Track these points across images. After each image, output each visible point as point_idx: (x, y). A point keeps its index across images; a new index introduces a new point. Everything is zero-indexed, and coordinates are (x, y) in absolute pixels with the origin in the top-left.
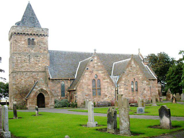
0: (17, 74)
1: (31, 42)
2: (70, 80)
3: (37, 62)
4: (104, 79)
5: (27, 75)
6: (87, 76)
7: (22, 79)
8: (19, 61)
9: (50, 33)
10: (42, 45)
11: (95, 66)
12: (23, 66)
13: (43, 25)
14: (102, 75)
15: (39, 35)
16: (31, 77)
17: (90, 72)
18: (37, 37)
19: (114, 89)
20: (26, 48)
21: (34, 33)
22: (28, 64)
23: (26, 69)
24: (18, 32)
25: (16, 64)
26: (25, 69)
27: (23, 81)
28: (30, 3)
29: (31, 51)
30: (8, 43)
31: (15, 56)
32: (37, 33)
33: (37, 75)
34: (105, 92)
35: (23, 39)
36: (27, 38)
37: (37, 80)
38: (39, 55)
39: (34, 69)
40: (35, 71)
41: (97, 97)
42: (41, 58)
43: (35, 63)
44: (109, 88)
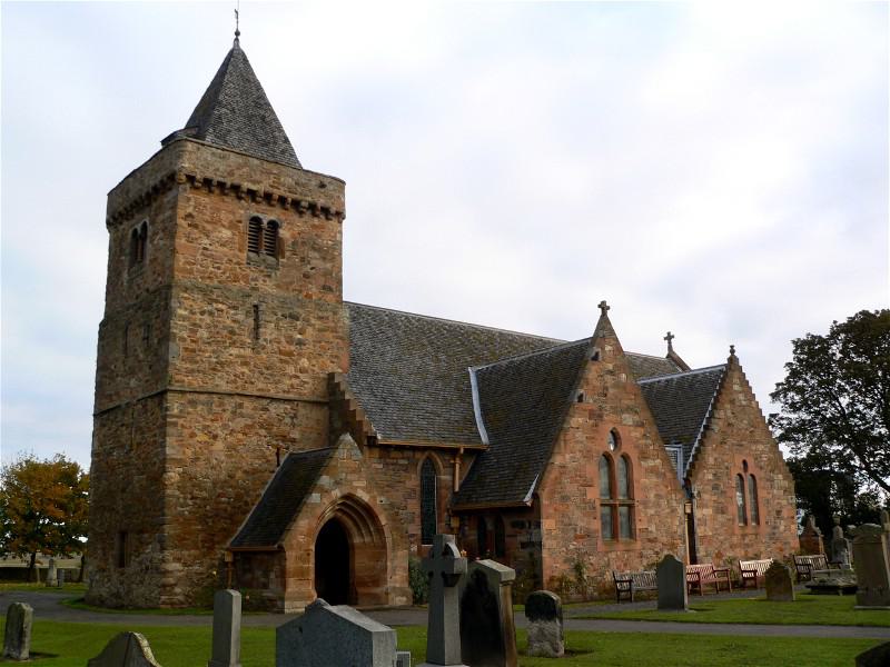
0: (193, 403)
1: (264, 239)
2: (462, 458)
3: (293, 348)
4: (644, 456)
5: (242, 416)
6: (579, 435)
7: (215, 437)
8: (203, 333)
9: (352, 202)
10: (314, 263)
11: (607, 389)
12: (222, 364)
13: (313, 154)
14: (637, 433)
15: (306, 205)
16: (262, 427)
17: (592, 414)
18: (293, 216)
19: (680, 511)
20: (238, 264)
21: (282, 192)
22: (248, 352)
23: (240, 382)
24: (209, 175)
25: (186, 349)
26: (235, 382)
27: (219, 446)
28: (243, 46)
29: (260, 284)
30: (102, 239)
31: (188, 303)
32: (295, 196)
33: (288, 420)
34: (649, 522)
35: (224, 217)
36: (245, 211)
37: (287, 448)
38: (301, 311)
39: (279, 382)
40: (281, 395)
41: (621, 547)
42: (310, 330)
43: (281, 352)
44: (664, 503)
